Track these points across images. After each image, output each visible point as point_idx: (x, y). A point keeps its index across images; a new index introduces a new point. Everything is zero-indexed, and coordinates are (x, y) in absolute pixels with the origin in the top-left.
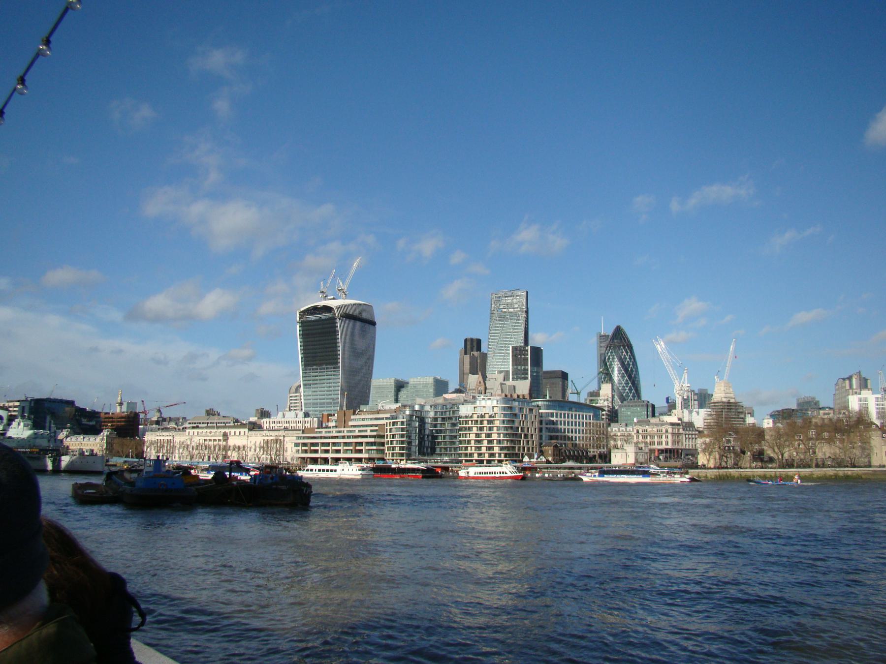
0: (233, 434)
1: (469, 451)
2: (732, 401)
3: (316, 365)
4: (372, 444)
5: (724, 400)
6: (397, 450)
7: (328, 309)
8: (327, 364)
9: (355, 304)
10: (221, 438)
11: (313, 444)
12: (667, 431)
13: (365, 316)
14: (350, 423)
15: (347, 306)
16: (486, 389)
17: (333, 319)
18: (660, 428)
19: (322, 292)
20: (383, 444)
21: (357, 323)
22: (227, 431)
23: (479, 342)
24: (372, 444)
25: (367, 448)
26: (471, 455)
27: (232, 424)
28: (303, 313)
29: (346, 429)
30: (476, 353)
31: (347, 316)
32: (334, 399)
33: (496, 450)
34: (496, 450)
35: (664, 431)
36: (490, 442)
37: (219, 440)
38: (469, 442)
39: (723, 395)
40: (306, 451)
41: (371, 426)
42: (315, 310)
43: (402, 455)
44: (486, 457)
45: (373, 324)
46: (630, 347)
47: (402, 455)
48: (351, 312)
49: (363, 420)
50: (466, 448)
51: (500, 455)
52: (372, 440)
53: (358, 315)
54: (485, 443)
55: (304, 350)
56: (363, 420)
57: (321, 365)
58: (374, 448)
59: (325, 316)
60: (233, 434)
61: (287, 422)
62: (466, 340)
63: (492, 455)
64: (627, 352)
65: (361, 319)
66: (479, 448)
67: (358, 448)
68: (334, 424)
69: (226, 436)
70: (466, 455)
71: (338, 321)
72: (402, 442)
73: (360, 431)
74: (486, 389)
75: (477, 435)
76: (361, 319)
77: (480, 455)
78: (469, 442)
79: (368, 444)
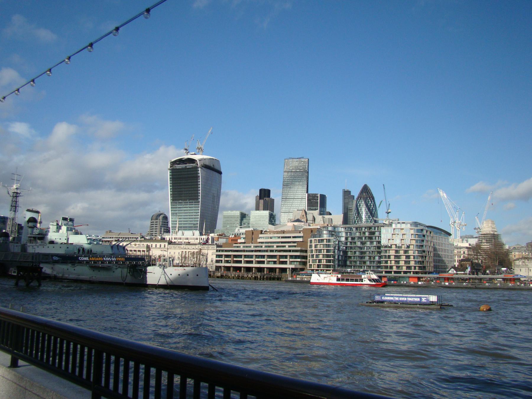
0: (154, 246)
1: (389, 264)
2: (496, 233)
3: (181, 200)
4: (296, 257)
5: (492, 233)
6: (324, 262)
7: (192, 161)
8: (190, 199)
9: (210, 159)
10: (145, 249)
11: (281, 256)
12: (464, 253)
13: (216, 167)
14: (259, 240)
15: (205, 159)
16: (307, 220)
17: (196, 168)
18: (459, 250)
19: (186, 149)
20: (305, 257)
21: (209, 171)
22: (149, 244)
23: (269, 191)
24: (296, 257)
25: (269, 260)
26: (391, 267)
27: (139, 239)
28: (173, 163)
29: (252, 245)
30: (267, 199)
31: (206, 167)
32: (194, 224)
33: (412, 264)
34: (412, 264)
35: (462, 252)
36: (408, 257)
37: (144, 251)
38: (389, 257)
39: (490, 229)
40: (275, 262)
41: (266, 243)
42: (181, 161)
43: (328, 266)
44: (404, 269)
45: (220, 173)
46: (373, 198)
47: (328, 266)
48: (207, 163)
49: (271, 238)
50: (386, 262)
51: (415, 267)
52: (298, 254)
53: (212, 166)
54: (403, 258)
55: (173, 189)
56: (271, 238)
57: (186, 200)
58: (299, 260)
59: (189, 166)
60: (154, 246)
61: (187, 239)
62: (261, 190)
63: (409, 268)
64: (371, 202)
65: (213, 169)
66: (397, 262)
67: (281, 260)
68: (243, 241)
69: (148, 248)
70: (386, 267)
71: (200, 169)
72: (328, 256)
73: (289, 246)
74: (307, 220)
75: (397, 251)
76: (213, 169)
77: (398, 267)
78: (389, 257)
79: (291, 257)
